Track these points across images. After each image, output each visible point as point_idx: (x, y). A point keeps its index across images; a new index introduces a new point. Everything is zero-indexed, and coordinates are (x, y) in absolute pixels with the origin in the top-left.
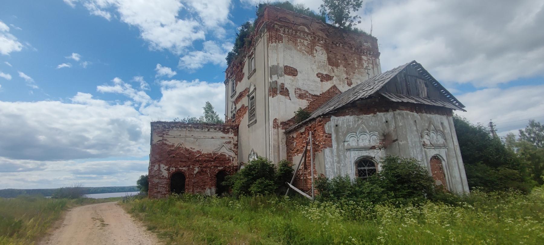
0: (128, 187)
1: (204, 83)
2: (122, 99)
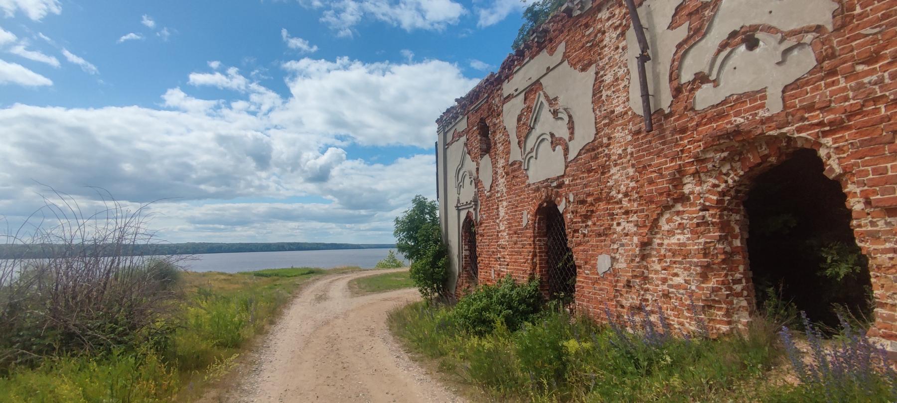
0: (275, 244)
1: (357, 64)
2: (227, 96)
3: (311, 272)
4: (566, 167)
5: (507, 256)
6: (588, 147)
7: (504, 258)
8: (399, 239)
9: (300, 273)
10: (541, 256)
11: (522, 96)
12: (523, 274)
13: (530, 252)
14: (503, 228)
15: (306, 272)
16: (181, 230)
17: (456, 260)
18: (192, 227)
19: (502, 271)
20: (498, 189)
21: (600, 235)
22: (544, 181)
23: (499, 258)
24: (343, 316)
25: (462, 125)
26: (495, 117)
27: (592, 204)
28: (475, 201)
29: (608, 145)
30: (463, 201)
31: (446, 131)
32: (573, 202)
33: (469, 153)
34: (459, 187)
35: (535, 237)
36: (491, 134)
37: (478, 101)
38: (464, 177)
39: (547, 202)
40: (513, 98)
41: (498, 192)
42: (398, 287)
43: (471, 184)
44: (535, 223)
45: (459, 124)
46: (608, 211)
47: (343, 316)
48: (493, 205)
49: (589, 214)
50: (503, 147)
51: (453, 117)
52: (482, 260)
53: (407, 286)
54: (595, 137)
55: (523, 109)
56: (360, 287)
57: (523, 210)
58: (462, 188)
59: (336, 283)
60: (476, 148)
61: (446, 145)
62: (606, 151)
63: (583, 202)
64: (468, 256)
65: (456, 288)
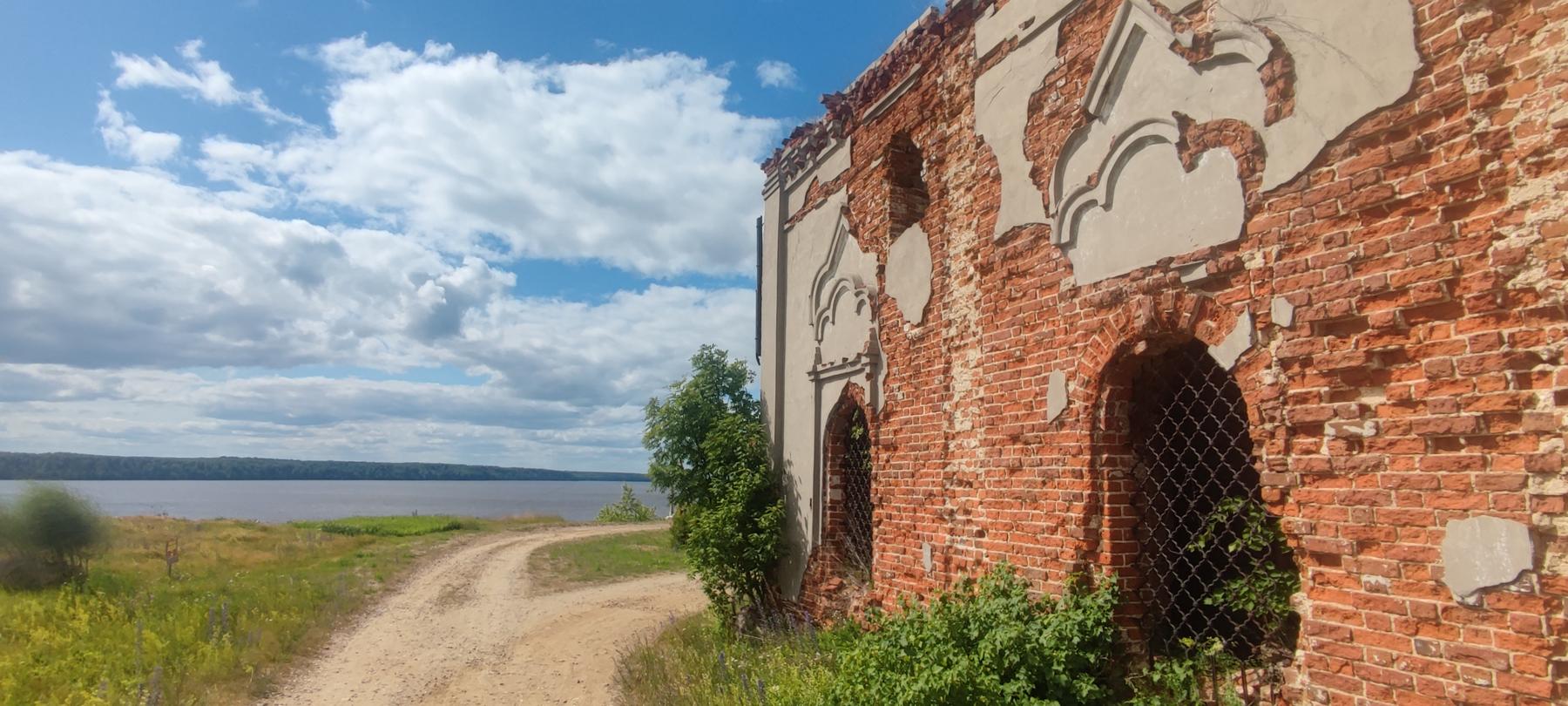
0: (399, 466)
3: (455, 527)
4: (1250, 213)
5: (980, 509)
6: (1368, 128)
7: (967, 512)
8: (656, 455)
9: (429, 527)
10: (1113, 512)
11: (1053, 32)
12: (1044, 564)
13: (1078, 497)
14: (967, 426)
15: (442, 527)
16: (192, 430)
17: (805, 513)
18: (213, 424)
19: (957, 552)
20: (947, 315)
21: (1445, 441)
22: (1147, 271)
23: (952, 513)
24: (493, 659)
25: (838, 162)
26: (945, 120)
27: (1392, 329)
28: (873, 353)
29: (1497, 98)
30: (832, 355)
31: (788, 186)
32: (1292, 328)
33: (854, 232)
34: (821, 323)
35: (1095, 451)
36: (929, 169)
37: (886, 92)
38: (836, 296)
39: (1149, 340)
40: (1011, 50)
41: (949, 324)
42: (645, 568)
43: (858, 311)
44: (1096, 406)
45: (824, 166)
46: (1505, 349)
47: (493, 659)
48: (930, 362)
49: (1375, 364)
50: (970, 197)
51: (809, 148)
52: (890, 517)
53: (666, 567)
54: (1415, 85)
55: (1053, 72)
56: (555, 568)
57: (1048, 369)
58: (829, 325)
59: (504, 555)
60: (874, 216)
61: (786, 222)
62: (1482, 124)
63: (1339, 326)
64: (838, 502)
65: (803, 587)
